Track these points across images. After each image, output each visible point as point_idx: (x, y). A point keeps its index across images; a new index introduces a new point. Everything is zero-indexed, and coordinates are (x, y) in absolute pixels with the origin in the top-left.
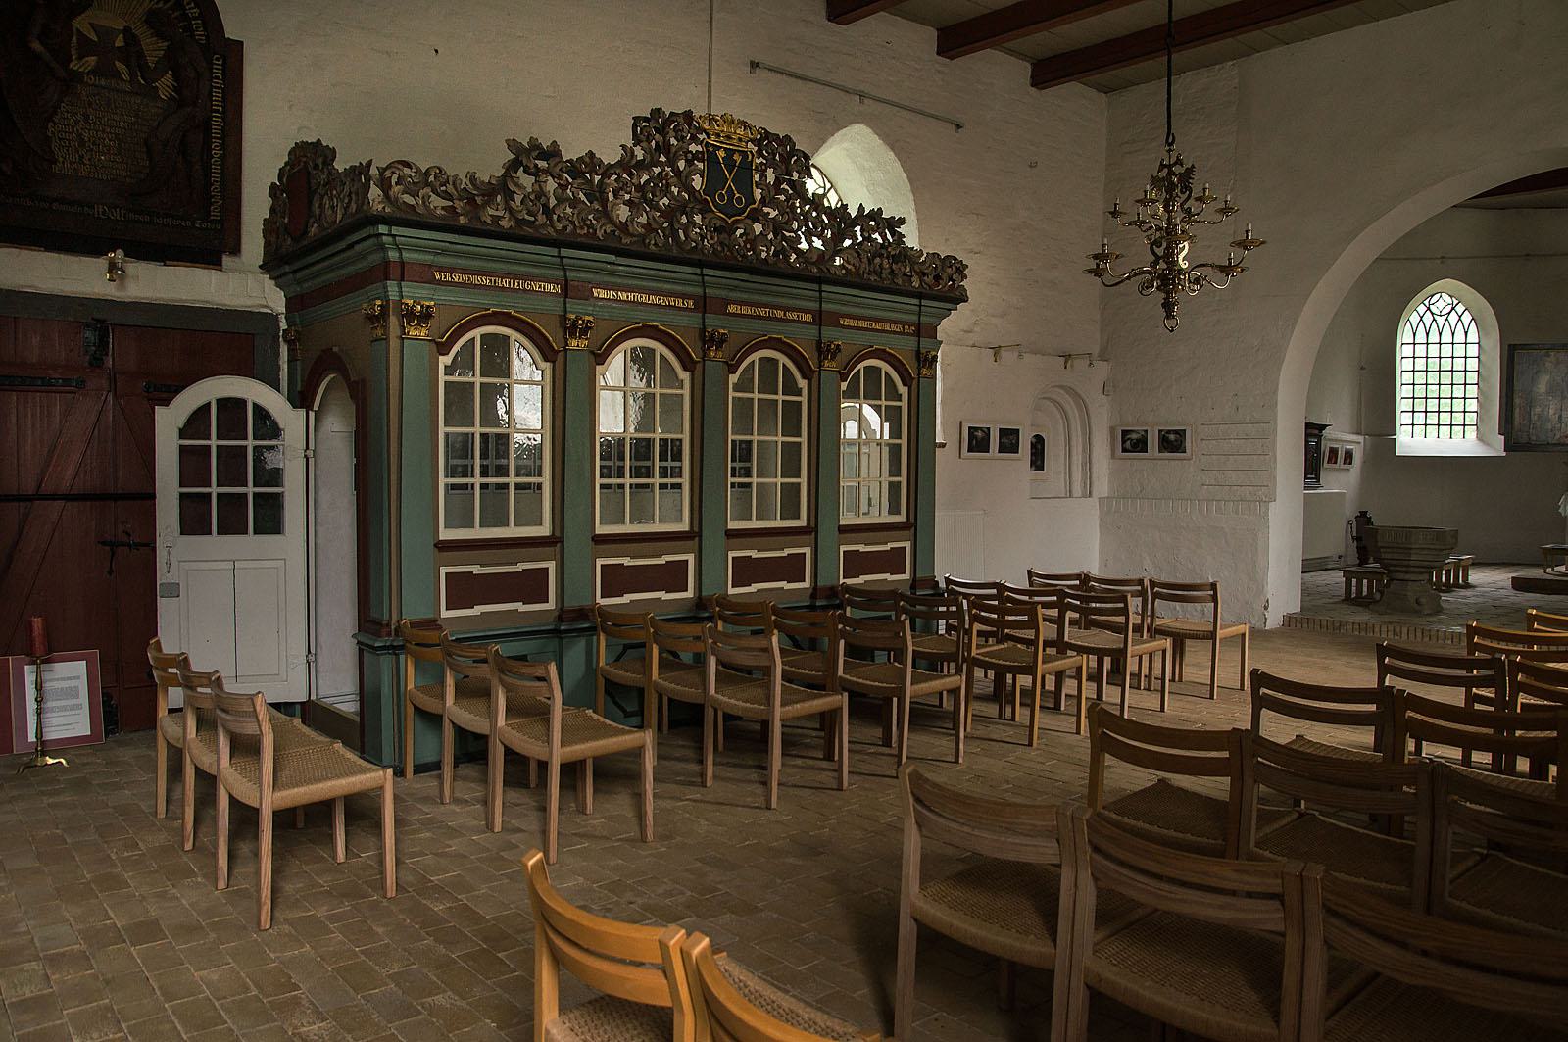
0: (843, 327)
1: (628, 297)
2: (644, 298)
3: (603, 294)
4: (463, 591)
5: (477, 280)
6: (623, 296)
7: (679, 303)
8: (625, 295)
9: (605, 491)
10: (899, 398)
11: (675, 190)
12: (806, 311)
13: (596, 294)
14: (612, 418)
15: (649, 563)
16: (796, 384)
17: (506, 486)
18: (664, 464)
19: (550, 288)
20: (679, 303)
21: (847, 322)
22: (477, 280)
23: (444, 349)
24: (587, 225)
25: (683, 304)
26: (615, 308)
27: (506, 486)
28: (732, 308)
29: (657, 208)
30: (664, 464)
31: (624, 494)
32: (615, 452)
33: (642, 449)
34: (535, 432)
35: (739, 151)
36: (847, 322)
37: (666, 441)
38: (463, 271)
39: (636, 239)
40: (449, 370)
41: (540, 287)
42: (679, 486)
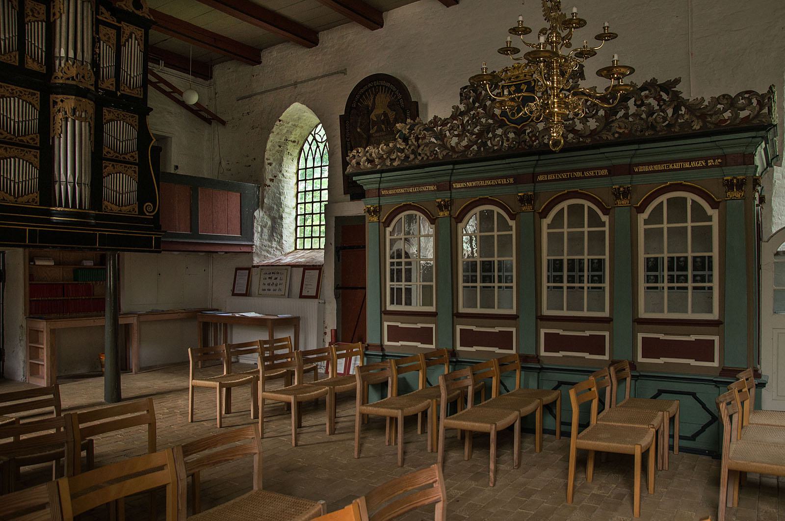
0: (639, 173)
1: (472, 184)
2: (482, 183)
3: (458, 186)
4: (396, 334)
5: (398, 191)
6: (469, 184)
7: (504, 181)
8: (471, 183)
9: (695, 291)
10: (510, 228)
11: (483, 120)
12: (601, 168)
13: (454, 187)
14: (467, 248)
15: (554, 332)
16: (706, 213)
17: (583, 288)
18: (671, 273)
19: (432, 188)
20: (504, 181)
21: (641, 169)
22: (398, 191)
23: (641, 209)
24: (434, 154)
25: (507, 181)
26: (463, 192)
27: (583, 288)
28: (540, 178)
29: (472, 134)
30: (671, 273)
31: (711, 297)
32: (577, 267)
33: (487, 267)
34: (430, 260)
35: (523, 83)
36: (641, 169)
37: (672, 258)
38: (393, 188)
39: (461, 154)
40: (646, 222)
41: (427, 188)
42: (511, 287)
